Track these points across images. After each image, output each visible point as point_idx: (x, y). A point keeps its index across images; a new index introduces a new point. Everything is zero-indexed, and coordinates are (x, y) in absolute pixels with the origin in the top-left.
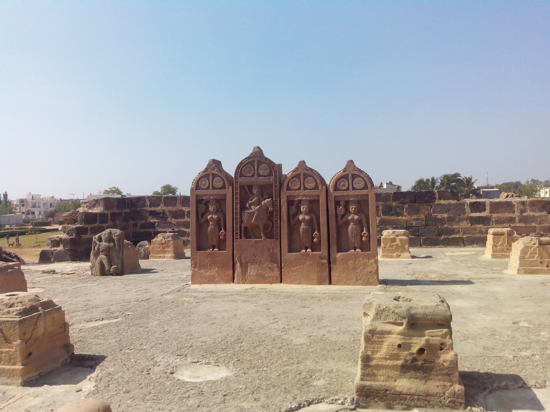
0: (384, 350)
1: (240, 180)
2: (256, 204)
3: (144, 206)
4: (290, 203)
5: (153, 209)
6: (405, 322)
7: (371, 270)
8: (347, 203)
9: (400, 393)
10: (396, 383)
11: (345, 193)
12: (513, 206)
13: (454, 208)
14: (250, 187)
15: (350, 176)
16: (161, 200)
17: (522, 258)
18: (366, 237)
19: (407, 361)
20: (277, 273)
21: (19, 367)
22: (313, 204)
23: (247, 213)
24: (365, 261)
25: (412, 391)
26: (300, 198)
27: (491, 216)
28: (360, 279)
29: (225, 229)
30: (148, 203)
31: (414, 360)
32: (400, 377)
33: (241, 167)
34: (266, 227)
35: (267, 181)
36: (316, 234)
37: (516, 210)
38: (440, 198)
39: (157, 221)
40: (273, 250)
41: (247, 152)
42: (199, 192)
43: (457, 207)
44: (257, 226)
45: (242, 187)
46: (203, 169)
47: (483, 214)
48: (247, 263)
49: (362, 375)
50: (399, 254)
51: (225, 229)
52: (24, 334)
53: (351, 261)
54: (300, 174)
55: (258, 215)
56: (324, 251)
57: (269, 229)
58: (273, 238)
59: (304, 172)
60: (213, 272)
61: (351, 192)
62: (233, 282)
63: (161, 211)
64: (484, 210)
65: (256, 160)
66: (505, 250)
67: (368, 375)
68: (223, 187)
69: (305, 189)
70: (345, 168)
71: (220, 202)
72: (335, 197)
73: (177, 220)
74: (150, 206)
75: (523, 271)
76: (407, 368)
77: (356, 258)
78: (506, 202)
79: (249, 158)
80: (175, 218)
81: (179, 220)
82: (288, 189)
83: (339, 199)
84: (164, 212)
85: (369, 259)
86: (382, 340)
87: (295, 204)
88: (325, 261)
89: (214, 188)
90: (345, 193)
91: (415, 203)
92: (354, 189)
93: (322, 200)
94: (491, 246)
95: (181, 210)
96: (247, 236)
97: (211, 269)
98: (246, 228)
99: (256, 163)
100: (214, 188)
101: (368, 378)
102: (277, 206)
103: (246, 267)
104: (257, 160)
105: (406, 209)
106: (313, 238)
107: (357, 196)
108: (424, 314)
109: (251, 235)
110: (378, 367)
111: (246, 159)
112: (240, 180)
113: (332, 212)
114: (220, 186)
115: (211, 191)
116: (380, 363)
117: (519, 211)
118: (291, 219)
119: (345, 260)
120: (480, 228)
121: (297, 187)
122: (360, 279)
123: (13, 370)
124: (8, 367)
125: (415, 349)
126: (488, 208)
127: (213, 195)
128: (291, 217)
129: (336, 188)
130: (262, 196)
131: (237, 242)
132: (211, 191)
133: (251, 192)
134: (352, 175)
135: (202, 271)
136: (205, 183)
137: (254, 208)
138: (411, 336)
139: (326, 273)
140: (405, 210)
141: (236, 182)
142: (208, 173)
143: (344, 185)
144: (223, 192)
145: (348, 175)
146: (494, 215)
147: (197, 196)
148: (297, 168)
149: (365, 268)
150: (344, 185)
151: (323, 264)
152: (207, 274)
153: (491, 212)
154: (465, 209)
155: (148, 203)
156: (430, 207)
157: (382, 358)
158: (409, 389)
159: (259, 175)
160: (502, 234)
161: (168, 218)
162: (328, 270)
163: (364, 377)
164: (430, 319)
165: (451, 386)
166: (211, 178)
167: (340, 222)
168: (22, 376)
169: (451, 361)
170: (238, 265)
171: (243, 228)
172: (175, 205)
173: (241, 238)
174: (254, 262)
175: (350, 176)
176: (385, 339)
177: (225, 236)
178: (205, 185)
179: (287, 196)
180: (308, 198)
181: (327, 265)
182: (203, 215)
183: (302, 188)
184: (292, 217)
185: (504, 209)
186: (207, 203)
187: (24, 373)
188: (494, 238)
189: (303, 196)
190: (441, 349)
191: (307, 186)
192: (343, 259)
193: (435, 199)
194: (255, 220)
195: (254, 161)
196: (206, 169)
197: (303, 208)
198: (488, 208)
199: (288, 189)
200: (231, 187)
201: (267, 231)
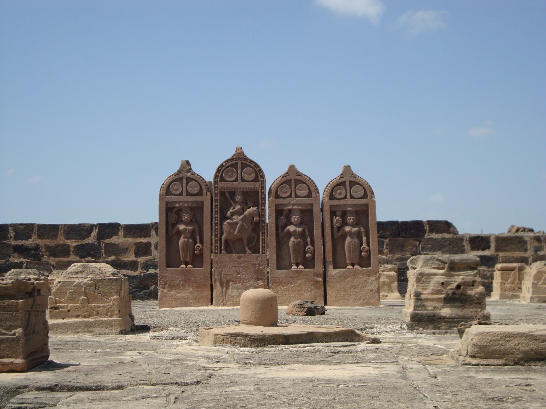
0: (431, 288)
1: (221, 185)
2: (240, 212)
3: (6, 238)
5: (20, 243)
6: (447, 265)
7: (372, 288)
8: (344, 214)
9: (445, 318)
10: (441, 311)
11: (343, 202)
12: (525, 242)
13: (449, 245)
14: (233, 194)
15: (348, 183)
16: (33, 230)
17: (534, 285)
18: (366, 252)
19: (448, 294)
22: (307, 214)
23: (228, 223)
24: (364, 279)
25: (453, 316)
26: (290, 207)
27: (498, 255)
28: (360, 299)
29: (202, 242)
30: (12, 234)
31: (454, 293)
32: (443, 307)
33: (221, 172)
34: (250, 240)
36: (309, 248)
37: (529, 247)
38: (431, 231)
39: (25, 260)
40: (259, 267)
41: (229, 154)
42: (170, 198)
43: (453, 242)
44: (241, 240)
45: (222, 194)
47: (487, 253)
48: (228, 282)
49: (414, 307)
50: (386, 294)
51: (202, 242)
53: (349, 279)
54: (291, 180)
55: (242, 226)
56: (319, 267)
57: (254, 243)
58: (259, 253)
59: (294, 179)
60: (186, 293)
61: (349, 201)
62: (212, 304)
63: (33, 246)
64: (489, 247)
65: (239, 162)
66: (516, 288)
67: (419, 306)
68: (200, 193)
69: (297, 196)
70: (342, 174)
71: (196, 210)
72: (331, 206)
73: (57, 259)
74: (16, 239)
75: (536, 299)
76: (450, 300)
77: (355, 275)
78: (517, 237)
79: (231, 160)
80: (55, 256)
81: (62, 259)
84: (37, 248)
86: (429, 280)
87: (285, 214)
88: (320, 279)
90: (343, 202)
91: (399, 237)
92: (352, 197)
93: (316, 210)
94: (499, 285)
95: (64, 245)
96: (228, 250)
97: (183, 290)
98: (226, 241)
99: (239, 165)
100: (188, 194)
101: (420, 309)
103: (227, 287)
104: (239, 165)
105: (387, 245)
106: (305, 253)
107: (355, 205)
108: (460, 260)
110: (427, 300)
111: (227, 161)
112: (221, 185)
113: (327, 224)
114: (195, 192)
115: (185, 198)
116: (428, 297)
117: (532, 249)
118: (280, 231)
119: (343, 277)
120: (484, 270)
121: (287, 195)
122: (360, 299)
123: (112, 321)
124: (106, 319)
125: (454, 286)
126: (493, 245)
127: (188, 202)
128: (280, 228)
129: (332, 196)
130: (245, 204)
132: (185, 198)
133: (233, 199)
134: (350, 182)
135: (172, 292)
136: (177, 188)
137: (237, 218)
138: (451, 276)
140: (385, 247)
141: (215, 187)
142: (181, 176)
143: (340, 194)
144: (199, 198)
145: (345, 182)
146: (501, 254)
148: (287, 173)
150: (340, 194)
151: (317, 282)
152: (179, 295)
153: (497, 250)
154: (463, 246)
155: (12, 234)
156: (417, 243)
157: (430, 294)
158: (451, 314)
159: (243, 180)
160: (512, 269)
161: (42, 256)
163: (416, 307)
164: (465, 263)
165: (481, 311)
166: (185, 181)
167: (336, 235)
169: (481, 293)
171: (223, 240)
172: (55, 237)
173: (221, 253)
174: (235, 281)
175: (348, 183)
176: (431, 280)
177: (201, 250)
178: (177, 190)
180: (300, 208)
181: (322, 283)
182: (174, 225)
183: (293, 196)
184: (280, 228)
185: (513, 247)
188: (502, 274)
190: (473, 285)
191: (299, 193)
192: (340, 277)
193: (425, 232)
194: (238, 232)
195: (237, 163)
196: (179, 171)
197: (295, 219)
198: (493, 245)
200: (209, 193)
201: (251, 245)
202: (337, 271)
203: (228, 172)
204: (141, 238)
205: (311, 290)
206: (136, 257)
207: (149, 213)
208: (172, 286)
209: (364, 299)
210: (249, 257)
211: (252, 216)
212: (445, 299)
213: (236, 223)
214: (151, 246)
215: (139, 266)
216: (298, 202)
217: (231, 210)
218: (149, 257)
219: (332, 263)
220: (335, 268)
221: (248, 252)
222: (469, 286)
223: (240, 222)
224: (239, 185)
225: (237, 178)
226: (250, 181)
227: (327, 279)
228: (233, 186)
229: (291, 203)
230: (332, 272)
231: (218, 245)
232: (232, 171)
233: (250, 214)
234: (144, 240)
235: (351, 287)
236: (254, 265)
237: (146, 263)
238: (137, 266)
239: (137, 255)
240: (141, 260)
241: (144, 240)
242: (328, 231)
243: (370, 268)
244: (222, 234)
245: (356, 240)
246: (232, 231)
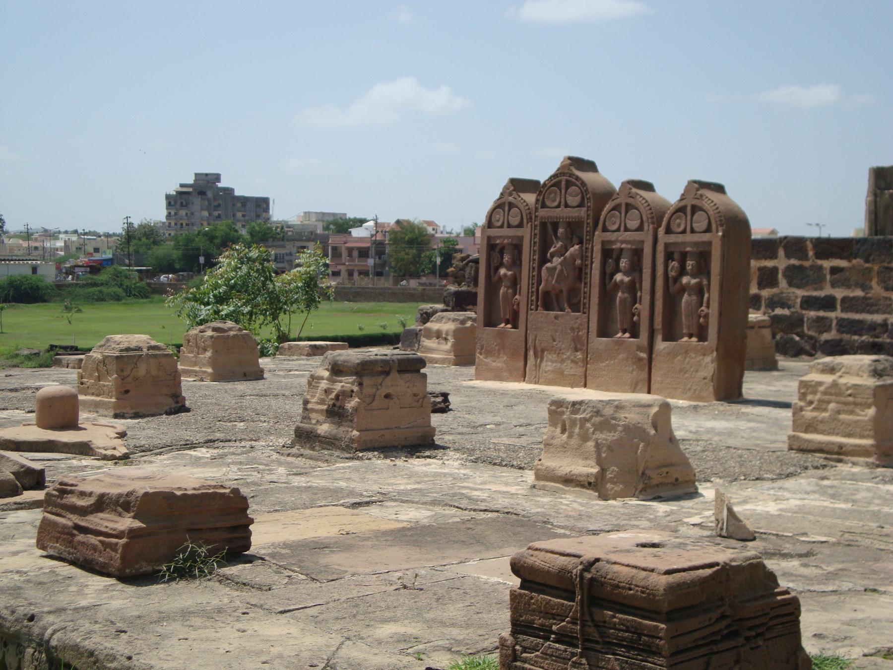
1: (542, 213)
2: (561, 253)
4: (607, 253)
7: (706, 375)
8: (684, 257)
15: (689, 208)
20: (580, 371)
21: (113, 400)
23: (547, 268)
26: (618, 245)
35: (576, 215)
42: (493, 232)
45: (543, 225)
46: (497, 196)
48: (543, 351)
51: (708, 307)
52: (122, 371)
53: (679, 358)
55: (561, 271)
60: (498, 363)
68: (520, 225)
70: (683, 195)
72: (667, 245)
77: (686, 352)
79: (555, 176)
82: (605, 229)
83: (672, 249)
85: (704, 355)
88: (644, 355)
89: (509, 226)
97: (498, 357)
102: (584, 256)
107: (696, 244)
109: (555, 305)
111: (551, 177)
112: (542, 213)
115: (505, 232)
118: (607, 281)
119: (672, 355)
122: (690, 389)
127: (508, 237)
131: (532, 315)
135: (488, 360)
136: (499, 217)
138: (334, 382)
139: (644, 375)
142: (503, 200)
144: (519, 232)
147: (489, 238)
149: (697, 371)
150: (679, 225)
151: (640, 359)
152: (494, 364)
162: (647, 370)
166: (506, 209)
167: (673, 289)
168: (115, 408)
170: (531, 353)
174: (551, 350)
179: (603, 243)
180: (629, 246)
181: (646, 362)
184: (606, 276)
186: (684, 257)
187: (116, 406)
189: (622, 242)
192: (669, 354)
194: (556, 281)
195: (560, 182)
196: (502, 194)
199: (605, 229)
200: (529, 225)
202: (668, 343)
203: (550, 194)
204: (766, 259)
205: (633, 371)
206: (759, 288)
207: (848, 219)
208: (489, 353)
209: (695, 390)
210: (569, 318)
211: (573, 258)
212: (327, 411)
213: (555, 268)
214: (777, 273)
215: (763, 303)
216: (628, 238)
217: (552, 250)
218: (775, 290)
219: (661, 331)
220: (666, 339)
221: (568, 310)
222: (348, 396)
223: (559, 267)
224: (563, 213)
225: (560, 203)
226: (574, 207)
227: (654, 356)
228: (555, 215)
229: (620, 238)
230: (661, 345)
231: (534, 298)
232: (555, 193)
233: (572, 255)
234: (769, 264)
235: (681, 371)
236: (572, 329)
237: (772, 299)
238: (760, 302)
239: (761, 286)
240: (766, 293)
241: (769, 264)
242: (660, 282)
243: (706, 343)
244: (539, 283)
245: (694, 298)
246: (550, 279)
